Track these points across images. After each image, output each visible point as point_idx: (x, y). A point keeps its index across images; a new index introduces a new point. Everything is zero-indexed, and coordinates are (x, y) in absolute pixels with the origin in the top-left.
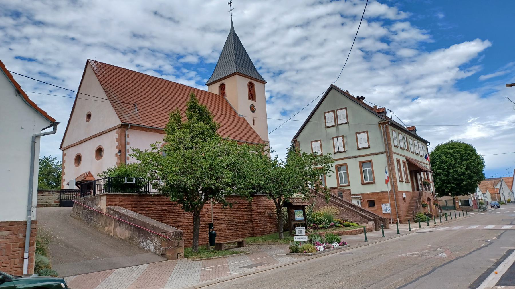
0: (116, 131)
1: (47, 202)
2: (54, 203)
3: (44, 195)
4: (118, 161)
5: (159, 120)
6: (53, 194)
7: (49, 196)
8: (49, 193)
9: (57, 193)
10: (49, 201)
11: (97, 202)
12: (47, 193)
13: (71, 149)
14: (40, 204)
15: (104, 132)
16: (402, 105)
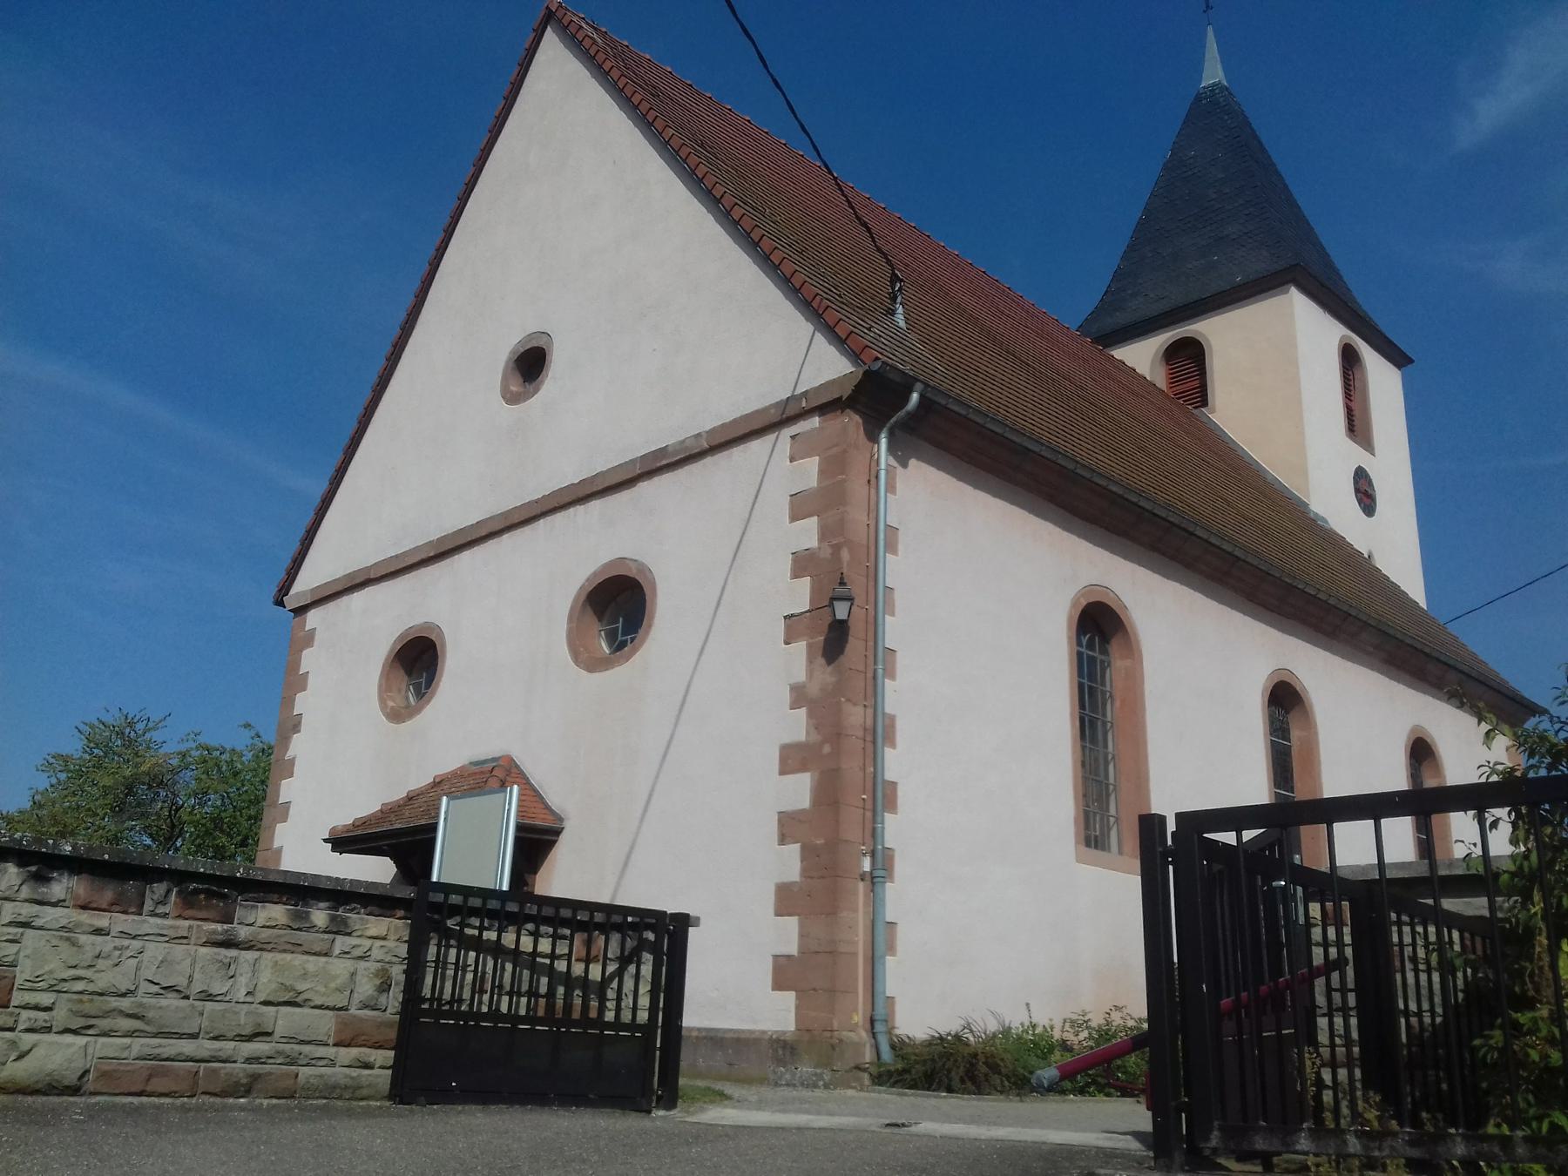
0: (793, 437)
1: (260, 1034)
2: (330, 1052)
3: (243, 933)
4: (810, 673)
5: (1026, 404)
6: (339, 928)
7: (295, 948)
8: (300, 921)
9: (378, 925)
10: (285, 1021)
11: (692, 1109)
12: (276, 912)
13: (357, 599)
14: (187, 1047)
15: (664, 457)
16: (10, 895)
